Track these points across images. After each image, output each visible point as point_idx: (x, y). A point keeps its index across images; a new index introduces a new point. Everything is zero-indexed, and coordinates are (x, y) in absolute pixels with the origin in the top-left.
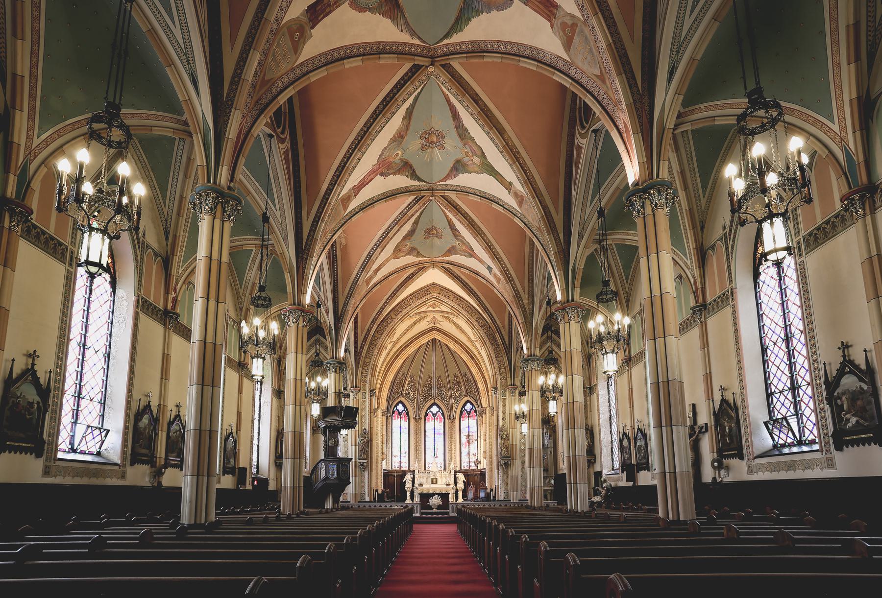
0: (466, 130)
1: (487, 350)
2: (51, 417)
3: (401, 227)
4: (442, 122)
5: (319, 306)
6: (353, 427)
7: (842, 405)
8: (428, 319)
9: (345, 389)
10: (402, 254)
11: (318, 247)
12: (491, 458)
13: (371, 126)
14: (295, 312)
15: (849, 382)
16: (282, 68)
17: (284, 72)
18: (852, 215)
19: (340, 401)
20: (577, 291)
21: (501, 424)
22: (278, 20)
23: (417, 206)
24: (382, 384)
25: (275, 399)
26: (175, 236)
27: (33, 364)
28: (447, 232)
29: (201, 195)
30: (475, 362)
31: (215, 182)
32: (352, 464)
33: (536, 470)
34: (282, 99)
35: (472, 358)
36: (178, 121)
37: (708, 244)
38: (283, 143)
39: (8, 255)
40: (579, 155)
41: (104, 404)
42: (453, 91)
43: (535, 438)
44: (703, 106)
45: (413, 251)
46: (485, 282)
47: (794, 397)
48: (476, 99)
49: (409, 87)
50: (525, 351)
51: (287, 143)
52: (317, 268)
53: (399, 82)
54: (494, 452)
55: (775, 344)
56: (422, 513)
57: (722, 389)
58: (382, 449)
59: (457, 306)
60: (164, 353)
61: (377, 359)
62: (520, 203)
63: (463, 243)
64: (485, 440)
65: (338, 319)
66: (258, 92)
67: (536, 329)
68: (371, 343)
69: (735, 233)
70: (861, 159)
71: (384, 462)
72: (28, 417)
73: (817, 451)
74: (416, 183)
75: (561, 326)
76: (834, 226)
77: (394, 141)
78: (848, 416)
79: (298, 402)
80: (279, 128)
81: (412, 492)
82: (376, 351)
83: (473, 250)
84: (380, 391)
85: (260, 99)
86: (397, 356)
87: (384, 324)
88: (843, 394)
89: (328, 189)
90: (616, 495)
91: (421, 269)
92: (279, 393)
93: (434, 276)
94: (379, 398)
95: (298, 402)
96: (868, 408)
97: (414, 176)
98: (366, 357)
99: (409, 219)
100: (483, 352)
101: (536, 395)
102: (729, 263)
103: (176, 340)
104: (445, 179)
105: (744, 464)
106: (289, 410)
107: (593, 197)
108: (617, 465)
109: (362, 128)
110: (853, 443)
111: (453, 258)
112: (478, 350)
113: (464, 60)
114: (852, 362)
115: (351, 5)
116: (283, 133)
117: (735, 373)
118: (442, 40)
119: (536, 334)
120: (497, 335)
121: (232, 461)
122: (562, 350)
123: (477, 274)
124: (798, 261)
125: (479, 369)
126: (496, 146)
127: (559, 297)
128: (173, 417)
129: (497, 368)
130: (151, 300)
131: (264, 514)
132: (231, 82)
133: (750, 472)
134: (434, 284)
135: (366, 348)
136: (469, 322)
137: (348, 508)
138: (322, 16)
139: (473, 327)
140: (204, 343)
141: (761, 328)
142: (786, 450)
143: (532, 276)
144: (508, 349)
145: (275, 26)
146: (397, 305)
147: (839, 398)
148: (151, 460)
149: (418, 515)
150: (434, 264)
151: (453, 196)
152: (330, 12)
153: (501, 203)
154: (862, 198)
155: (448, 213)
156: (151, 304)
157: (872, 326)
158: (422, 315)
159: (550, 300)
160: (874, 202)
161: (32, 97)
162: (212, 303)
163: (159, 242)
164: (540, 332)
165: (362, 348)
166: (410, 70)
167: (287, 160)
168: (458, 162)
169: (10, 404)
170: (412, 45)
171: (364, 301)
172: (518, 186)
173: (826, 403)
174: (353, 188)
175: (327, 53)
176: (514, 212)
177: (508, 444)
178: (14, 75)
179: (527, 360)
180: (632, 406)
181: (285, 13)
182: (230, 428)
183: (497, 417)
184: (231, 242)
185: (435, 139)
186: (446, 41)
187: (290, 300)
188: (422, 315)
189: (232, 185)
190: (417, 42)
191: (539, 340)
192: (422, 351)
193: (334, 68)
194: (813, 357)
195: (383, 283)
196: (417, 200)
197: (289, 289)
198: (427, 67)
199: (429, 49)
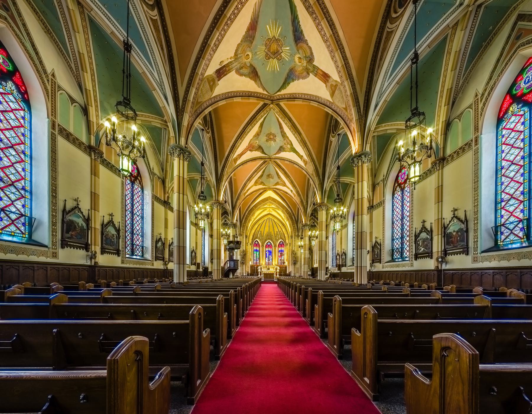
0: (285, 133)
1: (289, 222)
2: (122, 241)
3: (257, 173)
4: (275, 130)
5: (226, 202)
6: (239, 249)
7: (419, 244)
8: (267, 210)
9: (236, 235)
10: (258, 184)
11: (225, 178)
12: (289, 261)
13: (245, 129)
14: (216, 203)
15: (424, 235)
16: (206, 98)
17: (206, 99)
18: (434, 170)
19: (234, 239)
20: (326, 199)
21: (293, 249)
22: (202, 74)
23: (264, 165)
24: (250, 234)
25: (210, 238)
26: (166, 171)
27: (112, 219)
29: (173, 149)
30: (284, 227)
31: (179, 144)
32: (239, 262)
33: (306, 266)
34: (207, 112)
35: (283, 225)
36: (162, 120)
37: (376, 183)
38: (208, 134)
39: (96, 171)
40: (331, 145)
41: (143, 237)
42: (281, 116)
43: (306, 254)
44: (383, 125)
45: (262, 183)
46: (289, 196)
47: (402, 241)
48: (290, 120)
49: (262, 113)
50: (304, 223)
51: (210, 134)
52: (224, 187)
53: (257, 111)
54: (290, 259)
55: (397, 221)
56: (264, 280)
57: (376, 238)
58: (250, 257)
59: (278, 206)
60: (165, 218)
61: (248, 224)
62: (306, 164)
63: (282, 181)
64: (287, 255)
65: (233, 208)
66: (195, 107)
67: (308, 214)
68: (246, 218)
69: (388, 178)
70: (442, 146)
71: (251, 262)
72: (113, 240)
73: (408, 260)
74: (264, 155)
75: (319, 212)
76: (427, 175)
77: (255, 137)
78: (421, 248)
79: (218, 238)
80: (206, 127)
81: (261, 273)
82: (248, 221)
83: (285, 184)
84: (249, 236)
85: (196, 110)
86: (256, 224)
87: (251, 211)
88: (420, 240)
89: (228, 154)
90: (334, 276)
91: (265, 190)
92: (211, 236)
93: (270, 194)
94: (249, 239)
95: (218, 238)
96: (428, 245)
97: (263, 152)
98: (244, 223)
99: (261, 170)
100: (288, 223)
101: (307, 239)
102: (384, 190)
103: (169, 212)
104: (275, 154)
105: (381, 265)
106: (215, 241)
107: (335, 162)
108: (334, 265)
109: (242, 130)
110: (421, 257)
111: (278, 187)
112: (285, 222)
113: (286, 102)
114: (425, 227)
115: (236, 72)
116: (208, 129)
117: (382, 232)
119: (308, 216)
120: (293, 217)
121: (194, 260)
122: (319, 221)
123: (287, 193)
124: (411, 189)
125: (286, 229)
126: (298, 140)
127: (319, 202)
128: (170, 243)
129: (293, 229)
130: (158, 196)
131: (206, 280)
132: (183, 100)
134: (270, 197)
135: (244, 220)
136: (283, 211)
137: (238, 278)
138: (223, 75)
139: (284, 213)
140: (179, 211)
141: (393, 215)
142: (397, 260)
143: (308, 194)
144: (297, 222)
145: (201, 77)
146: (256, 204)
147: (419, 241)
148: (163, 259)
149: (263, 281)
150: (270, 189)
151: (278, 161)
152: (226, 74)
153: (298, 164)
154: (440, 162)
155: (276, 168)
156: (158, 198)
157: (435, 213)
158: (265, 209)
159: (314, 203)
160: (443, 164)
161: (96, 101)
162: (181, 195)
163: (160, 173)
164: (310, 215)
165: (242, 220)
166: (262, 106)
167: (210, 141)
168: (281, 147)
169: (105, 235)
170: (263, 94)
171: (243, 202)
172: (305, 157)
173: (414, 243)
174: (238, 155)
175: (226, 93)
176: (303, 168)
177: (296, 256)
178: (86, 89)
179: (305, 226)
180: (341, 244)
181: (206, 71)
182: (193, 248)
183: (292, 247)
184: (188, 175)
185: (272, 137)
186: (278, 93)
187: (214, 199)
188: (265, 209)
189: (187, 146)
190: (265, 93)
191: (309, 218)
192: (265, 222)
193: (229, 101)
194: (411, 226)
195: (251, 195)
196: (264, 162)
197: (214, 195)
198: (270, 105)
199: (271, 97)
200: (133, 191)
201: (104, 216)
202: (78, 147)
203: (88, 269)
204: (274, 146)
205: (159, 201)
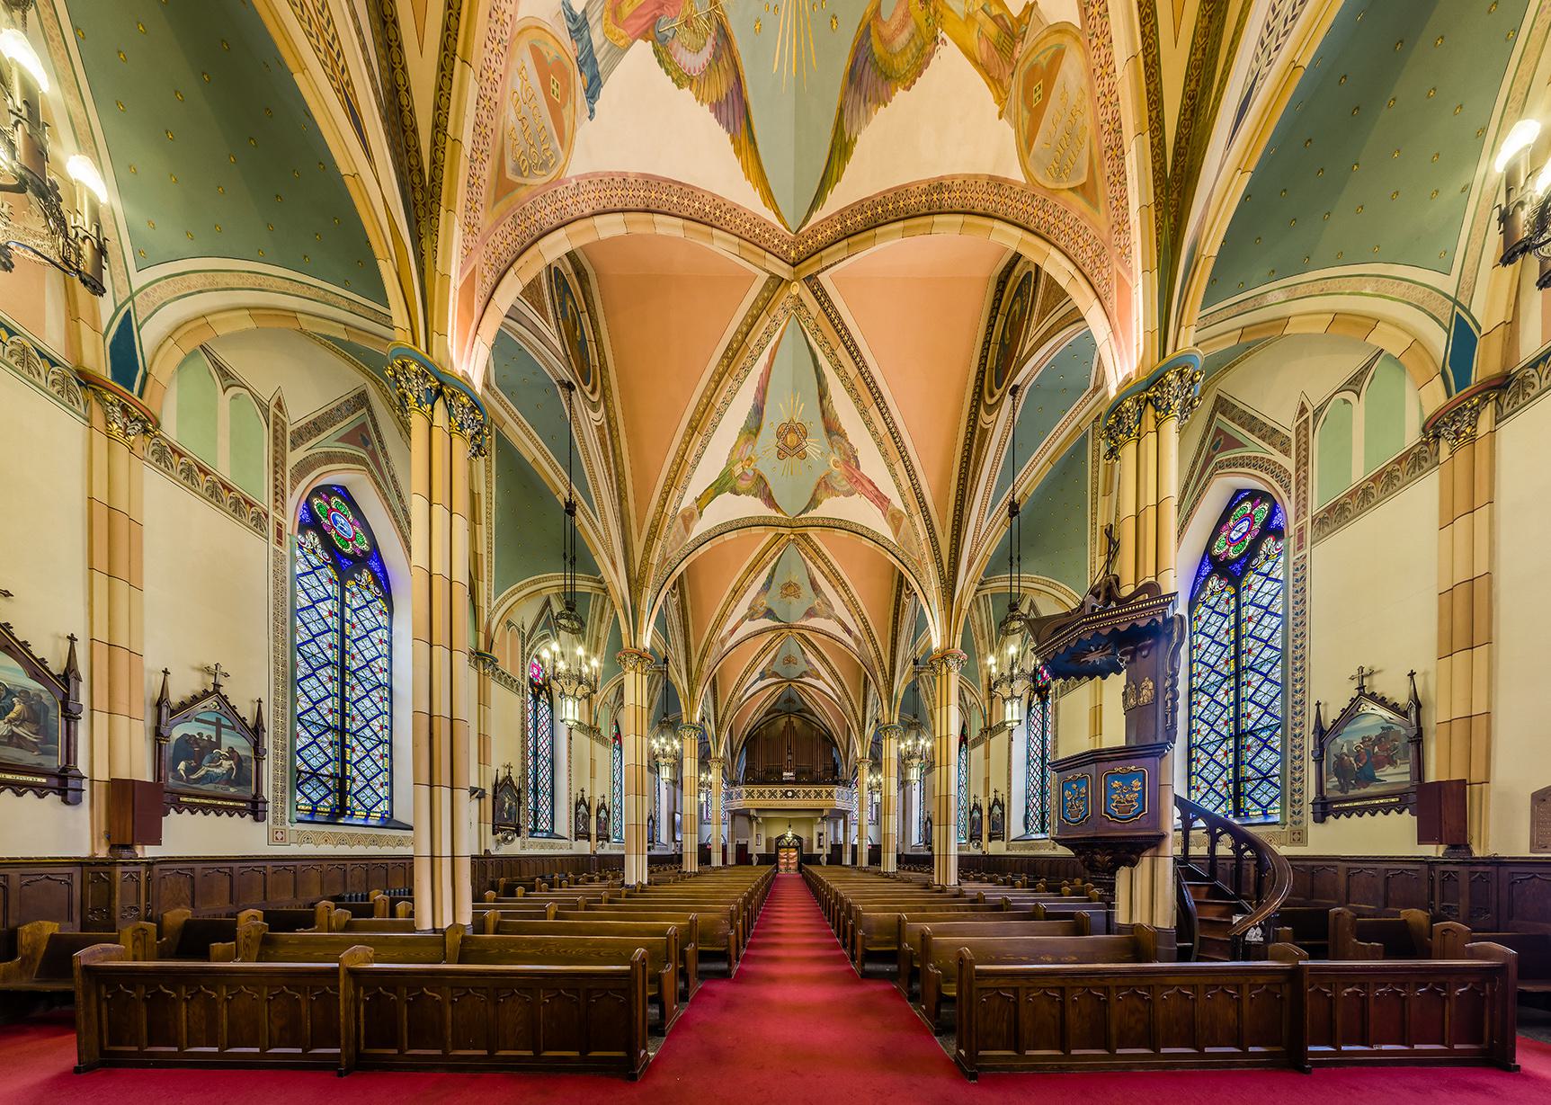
28: (806, 590)
36: (594, 581)
57: (996, 791)
80: (586, 385)
97: (770, 501)
116: (593, 392)
118: (800, 514)
133: (1008, 849)
198: (789, 283)
200: (536, 712)
201: (166, 672)
202: (54, 391)
203: (70, 875)
204: (797, 607)
205: (500, 678)
